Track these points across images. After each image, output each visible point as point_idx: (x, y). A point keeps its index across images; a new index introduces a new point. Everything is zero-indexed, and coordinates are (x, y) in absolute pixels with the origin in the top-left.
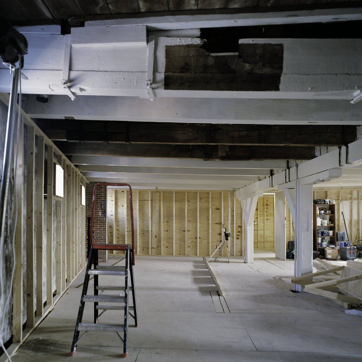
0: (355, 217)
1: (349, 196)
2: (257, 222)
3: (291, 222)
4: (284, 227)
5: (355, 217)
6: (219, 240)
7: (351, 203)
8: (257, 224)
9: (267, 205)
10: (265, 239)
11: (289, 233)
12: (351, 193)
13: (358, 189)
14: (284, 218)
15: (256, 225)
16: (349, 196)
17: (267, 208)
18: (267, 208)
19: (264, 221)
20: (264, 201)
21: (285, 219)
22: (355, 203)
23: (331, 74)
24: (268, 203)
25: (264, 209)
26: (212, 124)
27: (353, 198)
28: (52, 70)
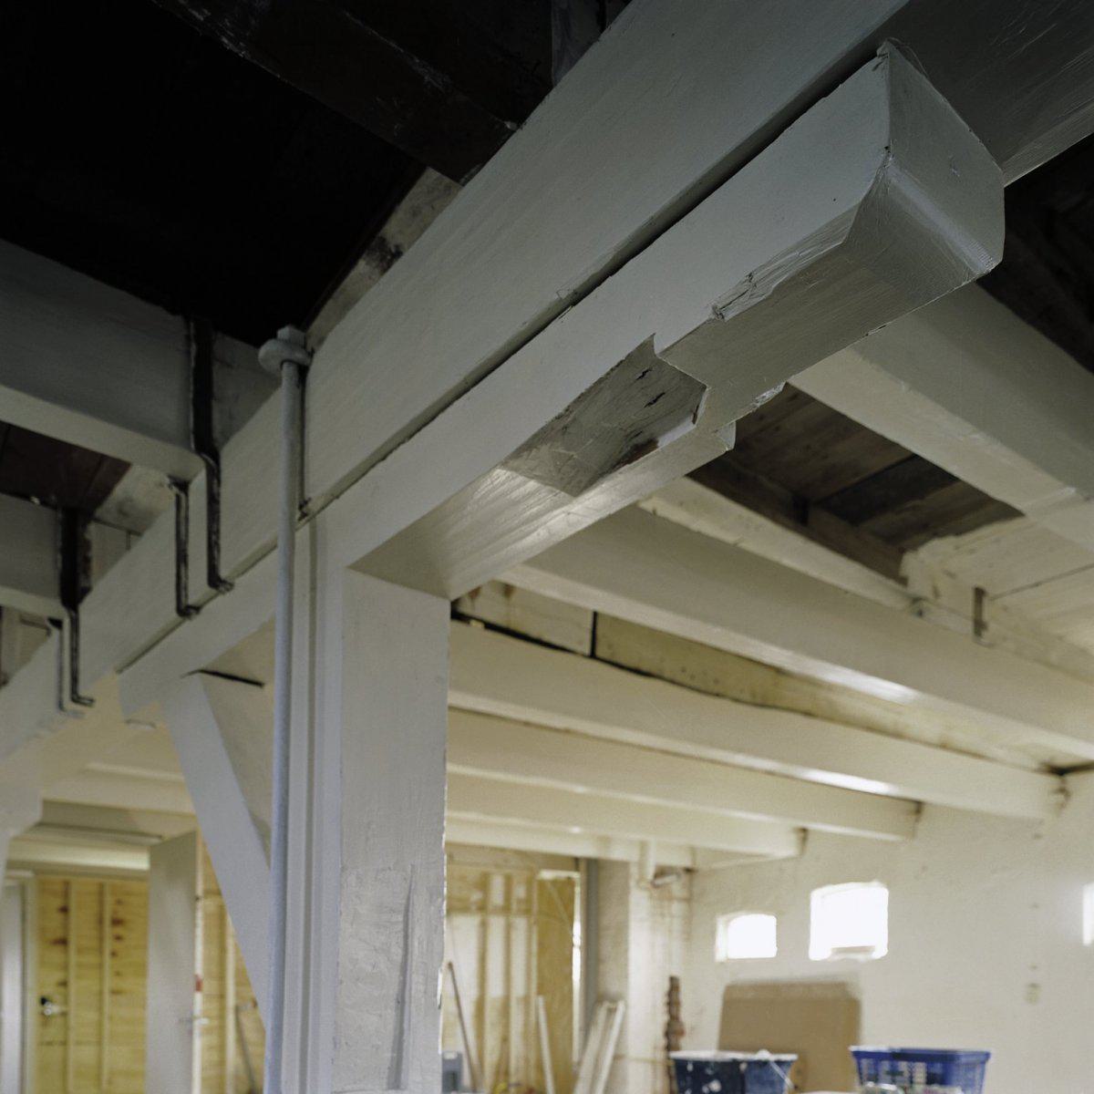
0: (495, 990)
1: (476, 896)
2: (66, 1002)
3: (231, 1001)
4: (191, 1032)
5: (495, 990)
6: (685, 878)
7: (484, 925)
8: (64, 1014)
9: (117, 922)
10: (105, 1085)
11: (215, 1057)
12: (483, 884)
13: (508, 871)
14: (192, 984)
15: (59, 1021)
16: (476, 896)
17: (118, 938)
18: (118, 938)
19: (101, 1000)
20: (101, 903)
21: (198, 987)
22: (497, 924)
23: (655, 401)
24: (121, 915)
25: (101, 939)
26: (610, 515)
27: (490, 907)
28: (577, 298)
